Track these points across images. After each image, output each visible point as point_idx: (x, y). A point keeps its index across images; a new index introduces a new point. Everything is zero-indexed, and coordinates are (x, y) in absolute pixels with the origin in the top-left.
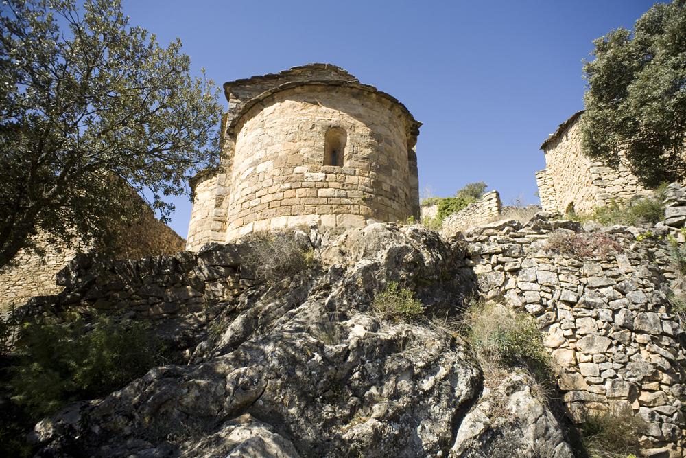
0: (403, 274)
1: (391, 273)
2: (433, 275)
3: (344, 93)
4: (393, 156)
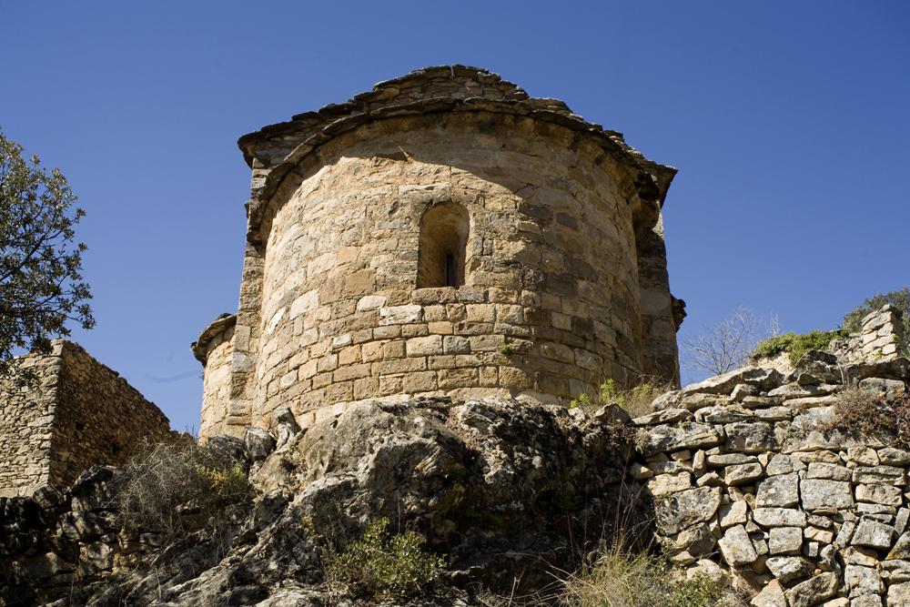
0: (411, 502)
1: (382, 501)
2: (509, 502)
3: (461, 125)
4: (581, 253)
